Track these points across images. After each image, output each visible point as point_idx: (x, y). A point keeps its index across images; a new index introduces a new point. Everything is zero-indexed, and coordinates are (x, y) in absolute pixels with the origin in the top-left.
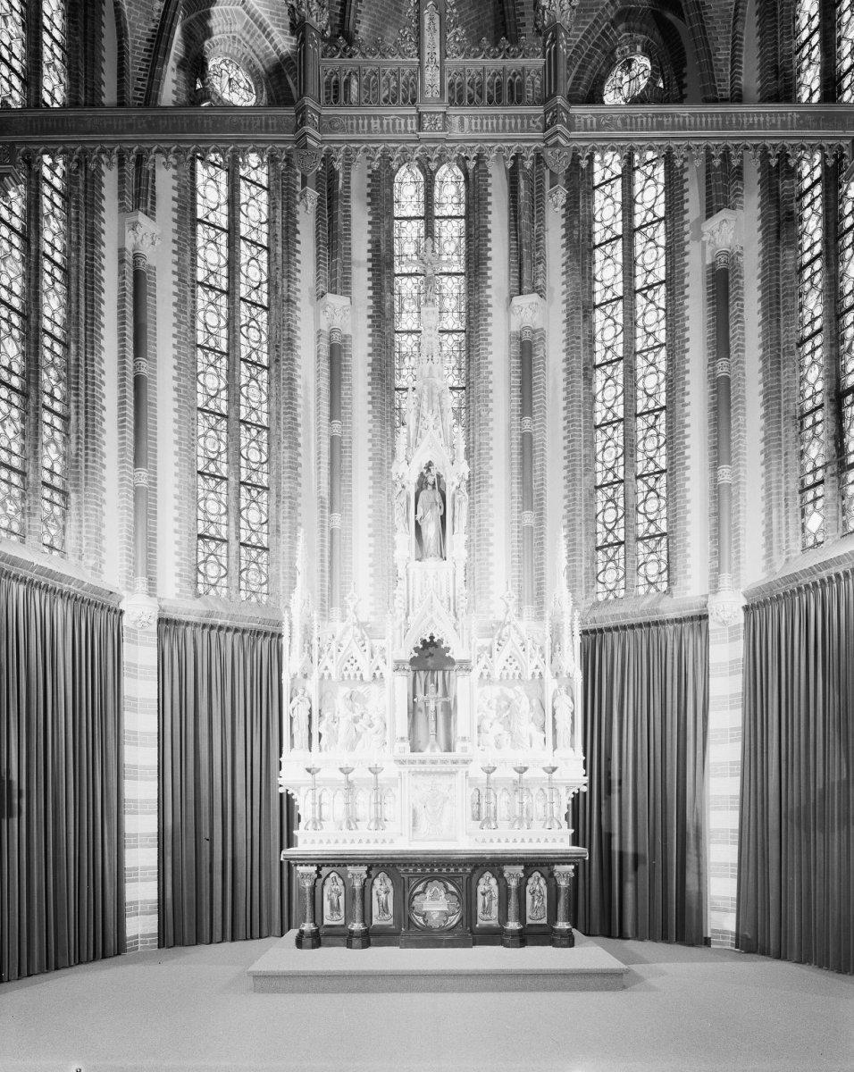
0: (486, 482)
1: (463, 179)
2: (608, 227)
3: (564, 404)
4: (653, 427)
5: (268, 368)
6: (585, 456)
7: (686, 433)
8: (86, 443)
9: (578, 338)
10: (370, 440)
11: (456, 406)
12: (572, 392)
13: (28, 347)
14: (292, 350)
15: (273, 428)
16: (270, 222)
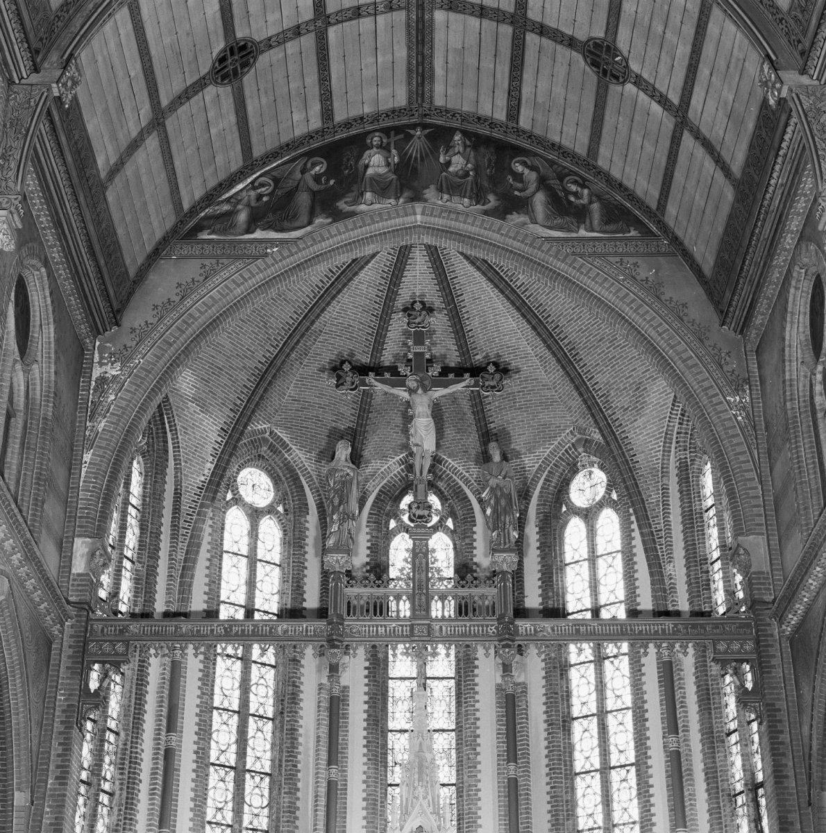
0: (475, 822)
1: (452, 546)
6: (567, 801)
9: (556, 693)
10: (364, 782)
11: (446, 747)
14: (296, 704)
16: (281, 593)
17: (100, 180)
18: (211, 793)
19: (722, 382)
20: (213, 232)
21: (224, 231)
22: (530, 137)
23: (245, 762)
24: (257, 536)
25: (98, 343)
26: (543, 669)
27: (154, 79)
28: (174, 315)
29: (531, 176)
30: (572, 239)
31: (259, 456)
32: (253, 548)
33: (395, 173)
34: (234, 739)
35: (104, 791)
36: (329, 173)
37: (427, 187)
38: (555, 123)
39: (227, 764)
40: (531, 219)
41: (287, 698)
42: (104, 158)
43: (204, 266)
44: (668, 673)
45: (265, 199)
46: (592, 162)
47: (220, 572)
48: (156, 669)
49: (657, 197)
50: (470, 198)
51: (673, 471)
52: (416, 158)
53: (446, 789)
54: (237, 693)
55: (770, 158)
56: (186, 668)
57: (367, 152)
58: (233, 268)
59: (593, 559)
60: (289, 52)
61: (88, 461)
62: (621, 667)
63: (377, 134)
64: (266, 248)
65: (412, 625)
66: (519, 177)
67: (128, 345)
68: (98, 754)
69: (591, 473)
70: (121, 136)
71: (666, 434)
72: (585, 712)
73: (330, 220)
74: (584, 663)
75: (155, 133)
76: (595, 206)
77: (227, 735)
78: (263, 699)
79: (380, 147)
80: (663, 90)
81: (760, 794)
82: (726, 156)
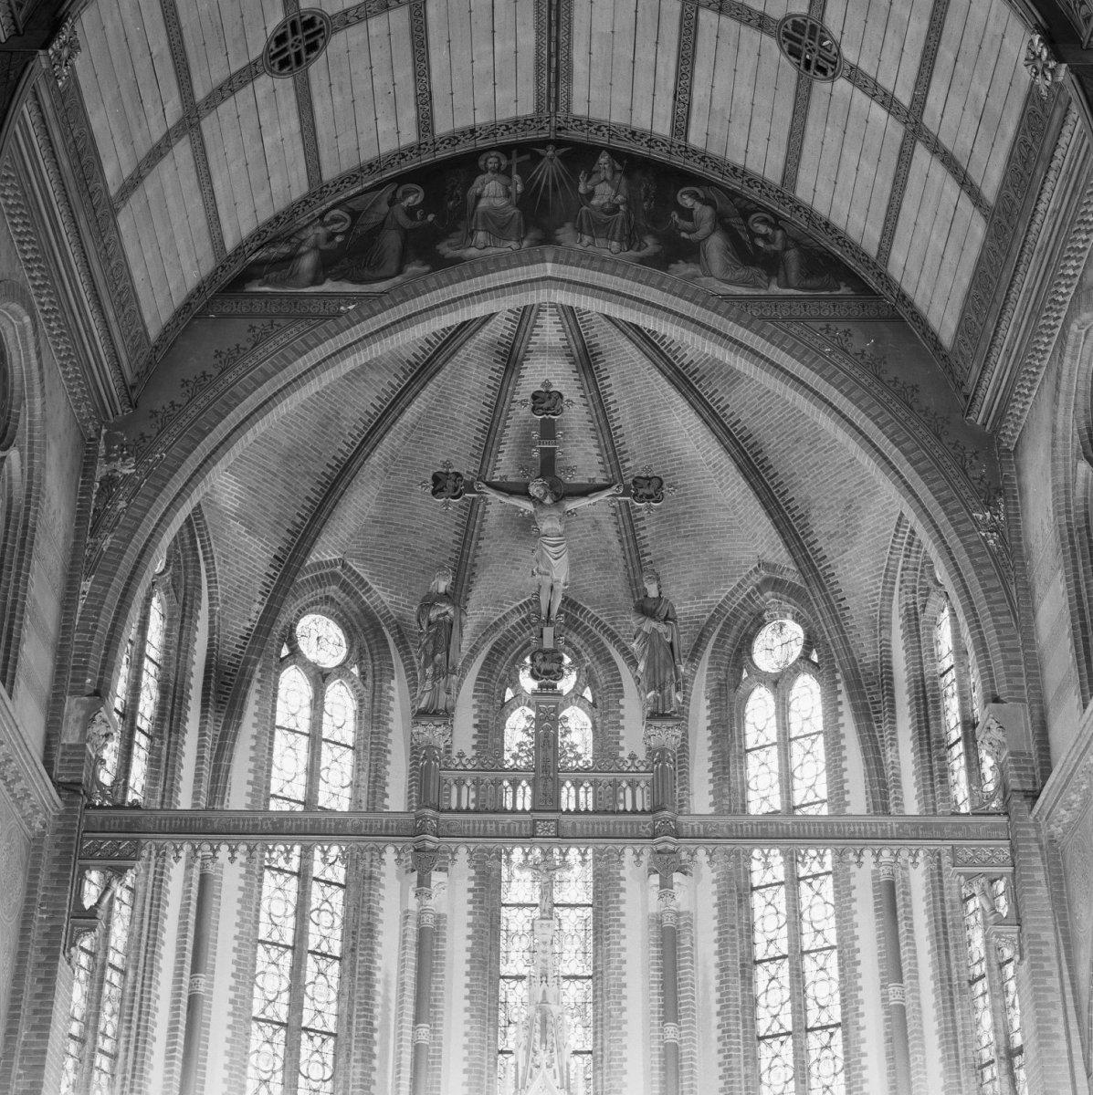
1: (590, 725)
2: (764, 798)
3: (717, 1007)
4: (827, 1047)
5: (340, 959)
6: (746, 1076)
7: (863, 1063)
8: (132, 1083)
9: (733, 927)
10: (466, 1047)
11: (580, 1000)
12: (728, 993)
13: (91, 987)
15: (342, 1035)
16: (355, 785)
17: (109, 199)
18: (253, 1059)
19: (965, 493)
20: (266, 283)
21: (282, 282)
22: (702, 159)
23: (301, 1018)
24: (322, 707)
25: (104, 431)
26: (714, 893)
27: (185, 59)
28: (211, 394)
29: (704, 213)
30: (759, 297)
31: (327, 597)
32: (316, 723)
33: (517, 206)
34: (285, 985)
35: (102, 1051)
36: (426, 206)
37: (562, 225)
38: (738, 139)
39: (276, 1019)
40: (703, 269)
41: (360, 930)
42: (115, 168)
43: (252, 328)
44: (890, 897)
45: (339, 239)
46: (788, 193)
47: (271, 754)
48: (176, 874)
49: (878, 239)
50: (621, 241)
51: (897, 622)
52: (546, 186)
53: (578, 1059)
54: (291, 922)
55: (1038, 172)
56: (220, 885)
57: (480, 178)
58: (292, 332)
59: (785, 741)
60: (373, 31)
61: (87, 590)
62: (823, 891)
63: (494, 154)
64: (340, 305)
65: (535, 821)
66: (687, 214)
67: (146, 434)
68: (95, 999)
69: (782, 626)
70: (138, 137)
71: (887, 570)
72: (772, 952)
73: (427, 268)
74: (771, 885)
75: (186, 139)
76: (792, 254)
77: (276, 978)
78: (327, 930)
79: (497, 171)
80: (889, 86)
81: (1017, 1065)
82: (975, 175)
